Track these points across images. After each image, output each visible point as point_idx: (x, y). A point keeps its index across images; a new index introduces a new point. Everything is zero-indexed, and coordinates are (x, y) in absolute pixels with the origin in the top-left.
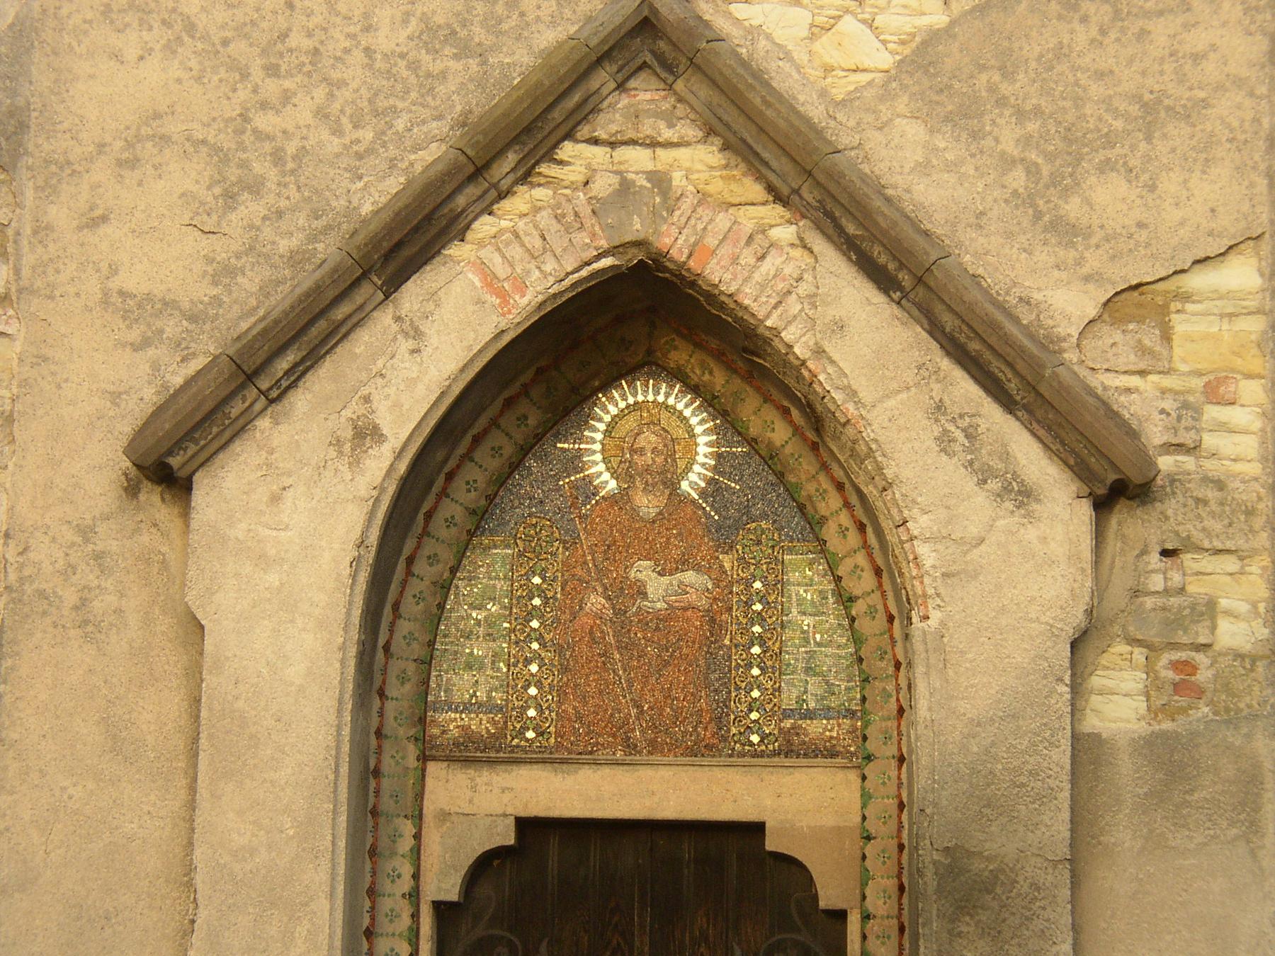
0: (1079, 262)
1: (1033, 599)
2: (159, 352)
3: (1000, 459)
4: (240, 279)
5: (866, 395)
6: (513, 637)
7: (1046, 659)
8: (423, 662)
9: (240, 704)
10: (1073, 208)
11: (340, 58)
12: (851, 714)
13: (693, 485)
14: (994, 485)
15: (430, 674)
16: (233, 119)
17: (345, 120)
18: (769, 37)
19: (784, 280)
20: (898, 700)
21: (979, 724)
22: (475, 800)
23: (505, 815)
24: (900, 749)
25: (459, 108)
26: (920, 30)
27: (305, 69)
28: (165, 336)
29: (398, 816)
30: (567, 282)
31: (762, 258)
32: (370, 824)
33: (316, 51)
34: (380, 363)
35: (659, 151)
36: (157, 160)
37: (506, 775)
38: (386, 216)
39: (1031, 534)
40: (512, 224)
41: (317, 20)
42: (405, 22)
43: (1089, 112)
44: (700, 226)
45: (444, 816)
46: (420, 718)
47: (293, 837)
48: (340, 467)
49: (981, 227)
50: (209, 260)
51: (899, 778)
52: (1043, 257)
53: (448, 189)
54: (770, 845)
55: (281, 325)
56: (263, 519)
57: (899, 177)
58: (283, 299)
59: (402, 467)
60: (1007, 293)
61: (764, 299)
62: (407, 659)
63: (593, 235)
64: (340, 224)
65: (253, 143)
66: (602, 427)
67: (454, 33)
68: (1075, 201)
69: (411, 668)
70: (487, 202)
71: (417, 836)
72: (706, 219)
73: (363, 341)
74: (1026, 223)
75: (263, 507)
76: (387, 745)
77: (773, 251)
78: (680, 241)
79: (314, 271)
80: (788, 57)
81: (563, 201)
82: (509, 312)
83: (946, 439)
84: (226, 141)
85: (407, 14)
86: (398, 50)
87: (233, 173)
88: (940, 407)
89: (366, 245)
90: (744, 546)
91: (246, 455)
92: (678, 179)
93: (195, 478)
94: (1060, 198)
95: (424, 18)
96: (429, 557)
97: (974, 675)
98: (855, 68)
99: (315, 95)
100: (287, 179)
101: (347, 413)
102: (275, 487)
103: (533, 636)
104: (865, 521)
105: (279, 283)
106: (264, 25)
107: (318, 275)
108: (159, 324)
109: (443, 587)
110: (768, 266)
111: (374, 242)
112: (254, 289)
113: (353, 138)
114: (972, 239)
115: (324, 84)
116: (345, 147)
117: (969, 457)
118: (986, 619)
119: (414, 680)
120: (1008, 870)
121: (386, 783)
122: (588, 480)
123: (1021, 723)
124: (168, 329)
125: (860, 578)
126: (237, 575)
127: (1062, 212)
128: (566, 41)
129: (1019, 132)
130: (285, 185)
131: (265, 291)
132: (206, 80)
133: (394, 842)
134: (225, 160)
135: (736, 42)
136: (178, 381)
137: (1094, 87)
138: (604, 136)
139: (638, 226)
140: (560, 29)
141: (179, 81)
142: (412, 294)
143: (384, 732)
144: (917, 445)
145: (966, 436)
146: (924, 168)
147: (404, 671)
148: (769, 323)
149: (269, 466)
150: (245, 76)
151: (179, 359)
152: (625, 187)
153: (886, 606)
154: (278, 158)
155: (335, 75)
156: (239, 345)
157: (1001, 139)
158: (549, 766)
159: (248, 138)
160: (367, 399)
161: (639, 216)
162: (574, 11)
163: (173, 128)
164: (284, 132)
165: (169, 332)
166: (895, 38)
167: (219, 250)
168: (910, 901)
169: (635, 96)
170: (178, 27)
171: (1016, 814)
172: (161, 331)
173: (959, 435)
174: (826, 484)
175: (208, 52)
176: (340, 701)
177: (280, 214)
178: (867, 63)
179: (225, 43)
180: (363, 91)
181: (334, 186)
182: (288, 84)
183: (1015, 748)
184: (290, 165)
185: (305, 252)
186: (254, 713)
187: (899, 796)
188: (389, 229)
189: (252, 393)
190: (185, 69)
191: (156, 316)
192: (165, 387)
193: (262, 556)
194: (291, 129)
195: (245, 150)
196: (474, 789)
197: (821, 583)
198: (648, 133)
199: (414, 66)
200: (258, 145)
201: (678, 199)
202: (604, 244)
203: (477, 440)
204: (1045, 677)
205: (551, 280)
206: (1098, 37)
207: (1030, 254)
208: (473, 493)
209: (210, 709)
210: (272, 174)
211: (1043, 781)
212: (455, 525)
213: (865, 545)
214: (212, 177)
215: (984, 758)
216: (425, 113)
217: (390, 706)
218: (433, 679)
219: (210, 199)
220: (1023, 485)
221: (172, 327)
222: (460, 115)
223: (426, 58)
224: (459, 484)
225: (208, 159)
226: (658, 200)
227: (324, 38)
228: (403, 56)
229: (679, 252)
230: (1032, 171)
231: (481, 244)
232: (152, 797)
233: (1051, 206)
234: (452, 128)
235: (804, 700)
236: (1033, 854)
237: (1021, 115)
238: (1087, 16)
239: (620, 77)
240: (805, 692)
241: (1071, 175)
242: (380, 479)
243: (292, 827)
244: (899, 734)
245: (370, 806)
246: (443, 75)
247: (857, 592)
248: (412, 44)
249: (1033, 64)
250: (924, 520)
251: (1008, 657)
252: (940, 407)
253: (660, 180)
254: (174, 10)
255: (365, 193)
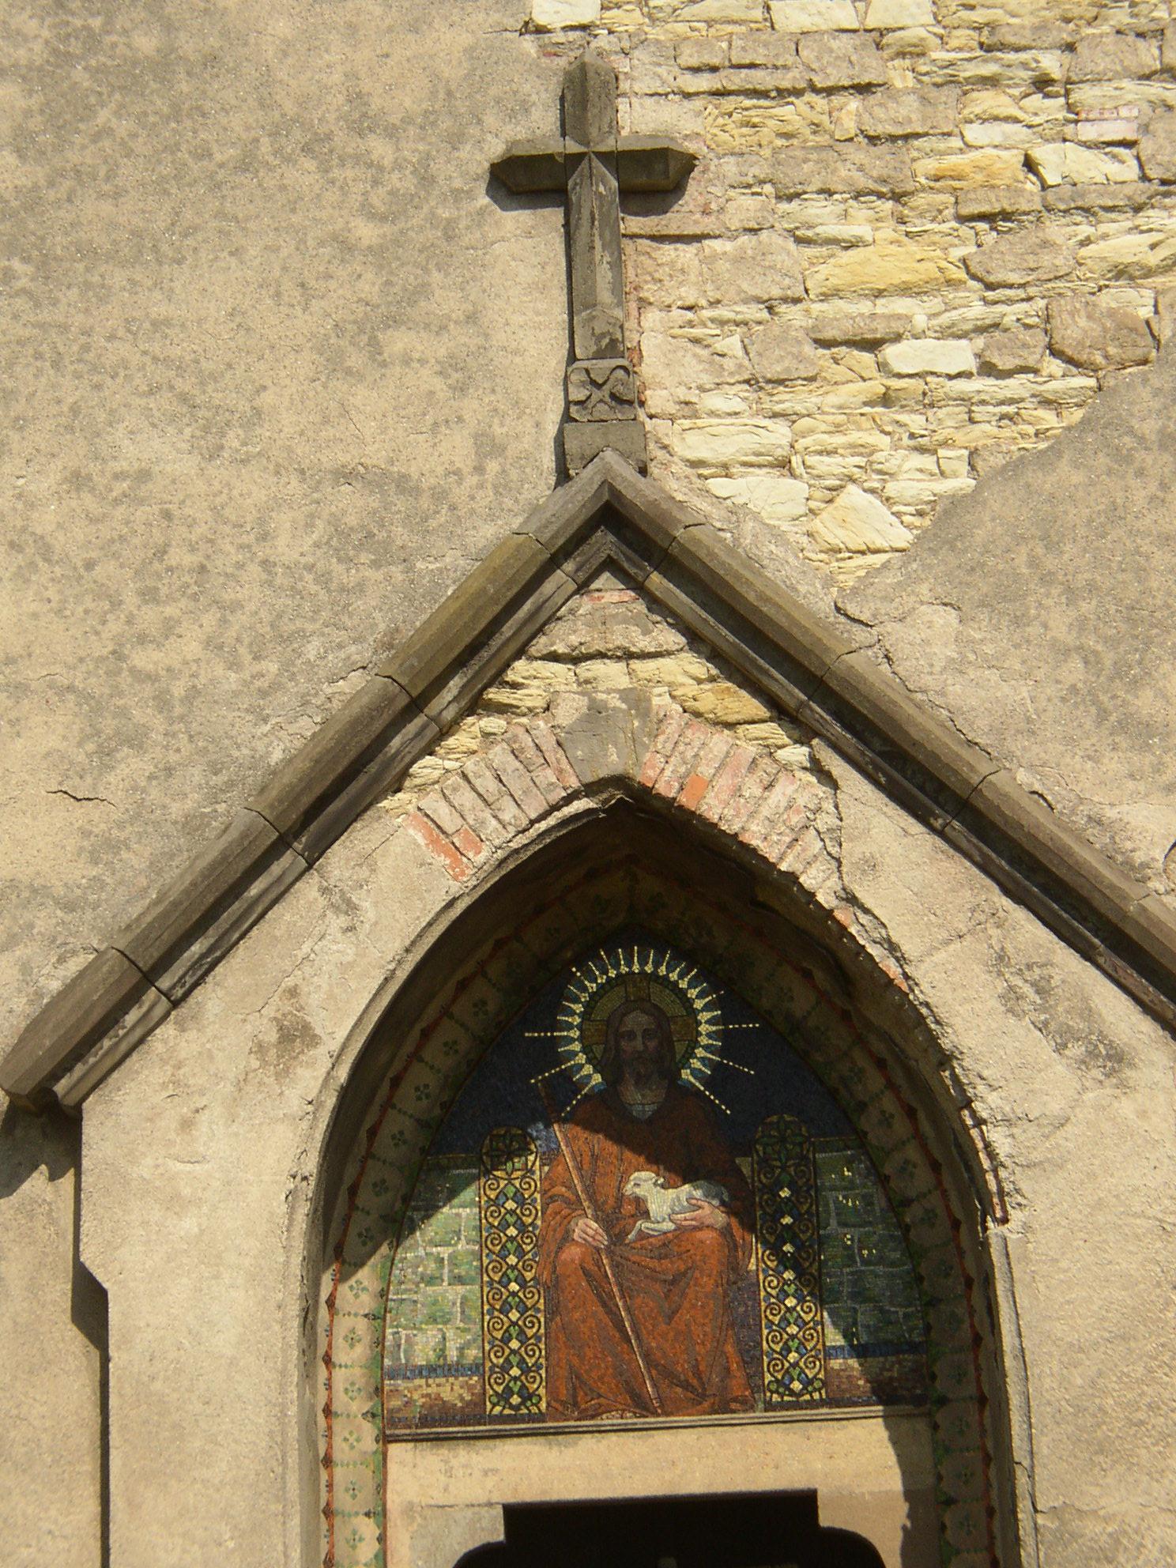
0: (1158, 768)
1: (1136, 1189)
2: (28, 951)
3: (1082, 1017)
4: (124, 855)
5: (907, 948)
6: (486, 1278)
7: (1158, 1263)
8: (375, 1318)
9: (158, 1385)
10: (1145, 703)
11: (233, 575)
12: (913, 1348)
13: (695, 1072)
14: (1076, 1050)
15: (384, 1332)
16: (102, 659)
17: (242, 650)
18: (756, 516)
19: (798, 812)
20: (972, 1326)
21: (1081, 1350)
22: (451, 1488)
23: (490, 1504)
24: (980, 1388)
25: (382, 627)
26: (941, 497)
27: (189, 591)
28: (35, 931)
29: (357, 1514)
30: (533, 833)
31: (769, 787)
32: (324, 1526)
33: (203, 569)
34: (306, 948)
35: (636, 664)
36: (13, 715)
37: (488, 1453)
38: (303, 765)
39: (1126, 1108)
40: (458, 764)
41: (201, 530)
42: (310, 526)
43: (1155, 585)
44: (690, 754)
45: (409, 1509)
46: (377, 1389)
47: (233, 1551)
48: (266, 1080)
49: (1034, 733)
50: (85, 834)
51: (981, 1424)
52: (1113, 764)
53: (378, 726)
54: (826, 1519)
55: (182, 907)
56: (173, 1151)
57: (929, 678)
58: (181, 876)
59: (343, 1074)
60: (1073, 812)
61: (775, 838)
62: (356, 1315)
63: (560, 772)
64: (245, 778)
65: (131, 685)
66: (578, 1008)
67: (370, 535)
68: (1147, 694)
69: (362, 1326)
70: (426, 739)
71: (382, 1539)
72: (697, 743)
73: (283, 917)
74: (1089, 724)
75: (172, 1136)
76: (338, 1425)
77: (783, 777)
78: (667, 773)
79: (219, 837)
80: (778, 536)
81: (521, 731)
82: (463, 873)
83: (1012, 995)
84: (97, 686)
85: (312, 516)
86: (303, 560)
87: (109, 725)
88: (1002, 958)
89: (281, 801)
90: (765, 1146)
91: (146, 1072)
92: (660, 700)
93: (85, 1105)
94: (1127, 692)
95: (334, 521)
96: (375, 1185)
97: (1069, 1288)
98: (864, 548)
99: (205, 622)
100: (176, 727)
101: (270, 1011)
102: (185, 1110)
103: (512, 1276)
104: (914, 1104)
105: (172, 856)
106: (136, 541)
107: (222, 844)
108: (28, 916)
109: (395, 1221)
110: (778, 796)
111: (291, 796)
112: (143, 866)
113: (255, 672)
114: (1024, 748)
115: (214, 609)
116: (246, 684)
117: (1042, 1017)
118: (1079, 1217)
119: (367, 1339)
120: (1130, 1531)
121: (339, 1472)
122: (567, 1075)
123: (1133, 1344)
124: (38, 922)
125: (912, 1175)
126: (145, 1224)
127: (1132, 709)
128: (508, 538)
129: (1073, 613)
130: (174, 735)
131: (155, 867)
132: (68, 613)
133: (354, 1547)
134: (98, 710)
135: (718, 525)
136: (55, 986)
137: (1158, 554)
138: (561, 648)
139: (615, 757)
140: (500, 522)
141: (35, 616)
142: (339, 859)
143: (334, 1408)
144: (977, 1006)
145: (1038, 992)
146: (957, 666)
147: (353, 1331)
148: (783, 867)
149: (176, 1083)
150: (116, 604)
151: (54, 960)
152: (596, 711)
153: (948, 1207)
154: (162, 702)
155: (228, 596)
156: (130, 936)
157: (1051, 624)
158: (541, 1439)
159: (125, 679)
160: (293, 992)
161: (615, 745)
162: (516, 501)
163: (31, 673)
164: (169, 670)
165: (40, 926)
166: (911, 509)
167: (96, 819)
168: (318, 1544)
169: (599, 598)
170: (30, 550)
171: (1135, 1460)
172: (31, 926)
173: (1028, 990)
174: (862, 1061)
175: (68, 578)
176: (283, 1373)
177: (169, 771)
178: (880, 543)
179: (90, 565)
180: (263, 614)
181: (234, 733)
182: (170, 610)
183: (1128, 1376)
184: (178, 710)
185: (204, 815)
186: (175, 1396)
187: (984, 1448)
188: (308, 780)
189: (152, 993)
190: (41, 600)
191: (25, 907)
192: (39, 994)
193: (176, 1197)
194: (177, 666)
195: (121, 694)
196: (449, 1472)
197: (864, 1186)
198: (618, 643)
199: (324, 579)
200: (137, 687)
201: (661, 721)
202: (574, 783)
203: (426, 1034)
204: (1159, 1284)
205: (512, 830)
206: (1159, 494)
207: (1097, 762)
208: (425, 1102)
209: (121, 1396)
210: (159, 723)
211: (1166, 1417)
212: (405, 1142)
213: (918, 1135)
214: (82, 730)
215: (1090, 1391)
216: (342, 636)
217: (339, 1375)
218: (389, 1337)
219: (81, 758)
220: (1112, 1048)
221: (45, 920)
222: (385, 635)
223: (338, 568)
224: (407, 1090)
225: (77, 709)
226: (636, 723)
227: (210, 551)
228: (310, 568)
229: (666, 787)
230: (1090, 660)
231: (421, 788)
232: (53, 1513)
233: (1119, 702)
234: (375, 652)
235: (853, 1334)
236: (1162, 1509)
237: (1071, 595)
238: (1143, 469)
239: (582, 576)
240: (855, 1324)
241: (1140, 662)
242: (315, 1091)
243: (232, 1538)
244: (978, 1368)
245: (323, 1504)
246: (360, 588)
247: (913, 1194)
248: (319, 553)
249: (1081, 531)
250: (993, 1098)
251: (1110, 1262)
252: (1002, 958)
253: (637, 701)
254: (24, 529)
255: (273, 738)
